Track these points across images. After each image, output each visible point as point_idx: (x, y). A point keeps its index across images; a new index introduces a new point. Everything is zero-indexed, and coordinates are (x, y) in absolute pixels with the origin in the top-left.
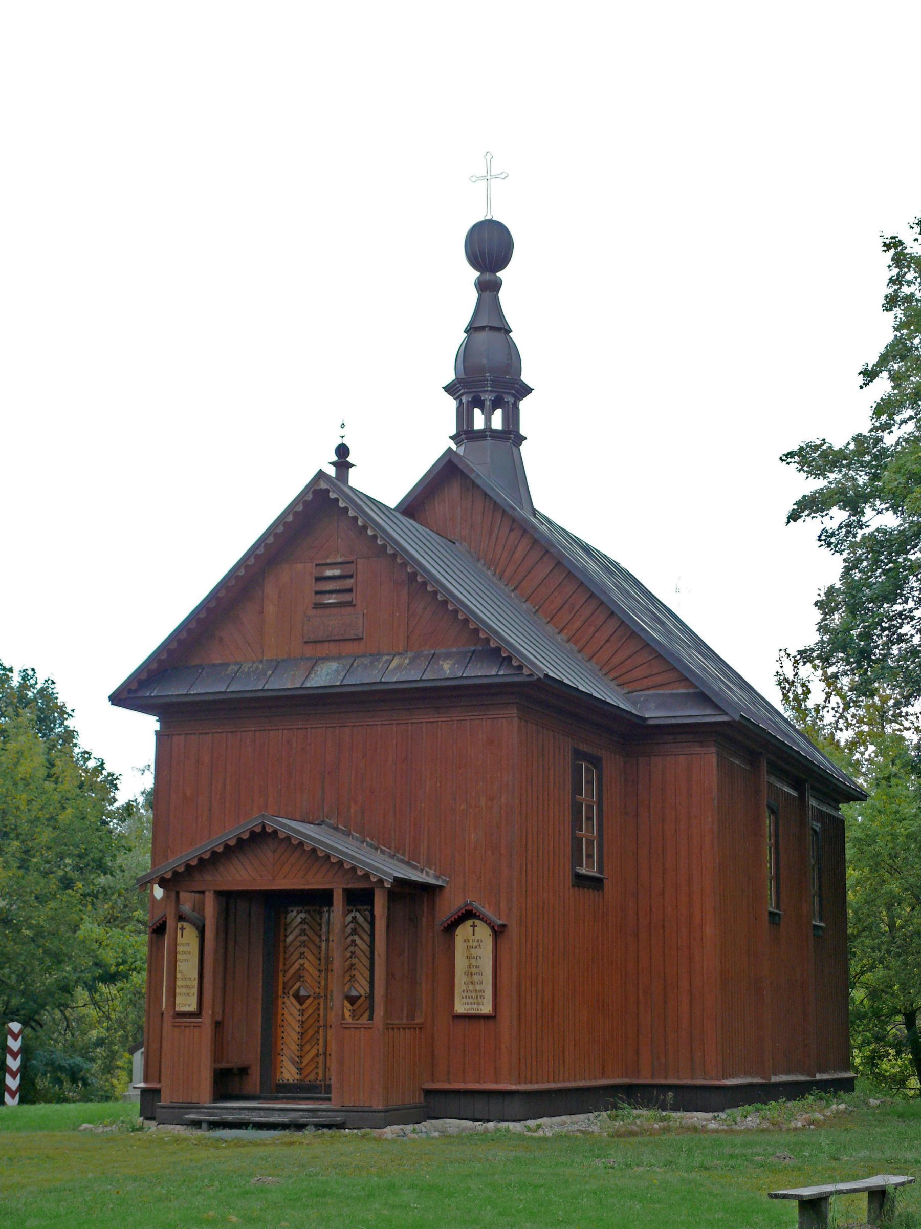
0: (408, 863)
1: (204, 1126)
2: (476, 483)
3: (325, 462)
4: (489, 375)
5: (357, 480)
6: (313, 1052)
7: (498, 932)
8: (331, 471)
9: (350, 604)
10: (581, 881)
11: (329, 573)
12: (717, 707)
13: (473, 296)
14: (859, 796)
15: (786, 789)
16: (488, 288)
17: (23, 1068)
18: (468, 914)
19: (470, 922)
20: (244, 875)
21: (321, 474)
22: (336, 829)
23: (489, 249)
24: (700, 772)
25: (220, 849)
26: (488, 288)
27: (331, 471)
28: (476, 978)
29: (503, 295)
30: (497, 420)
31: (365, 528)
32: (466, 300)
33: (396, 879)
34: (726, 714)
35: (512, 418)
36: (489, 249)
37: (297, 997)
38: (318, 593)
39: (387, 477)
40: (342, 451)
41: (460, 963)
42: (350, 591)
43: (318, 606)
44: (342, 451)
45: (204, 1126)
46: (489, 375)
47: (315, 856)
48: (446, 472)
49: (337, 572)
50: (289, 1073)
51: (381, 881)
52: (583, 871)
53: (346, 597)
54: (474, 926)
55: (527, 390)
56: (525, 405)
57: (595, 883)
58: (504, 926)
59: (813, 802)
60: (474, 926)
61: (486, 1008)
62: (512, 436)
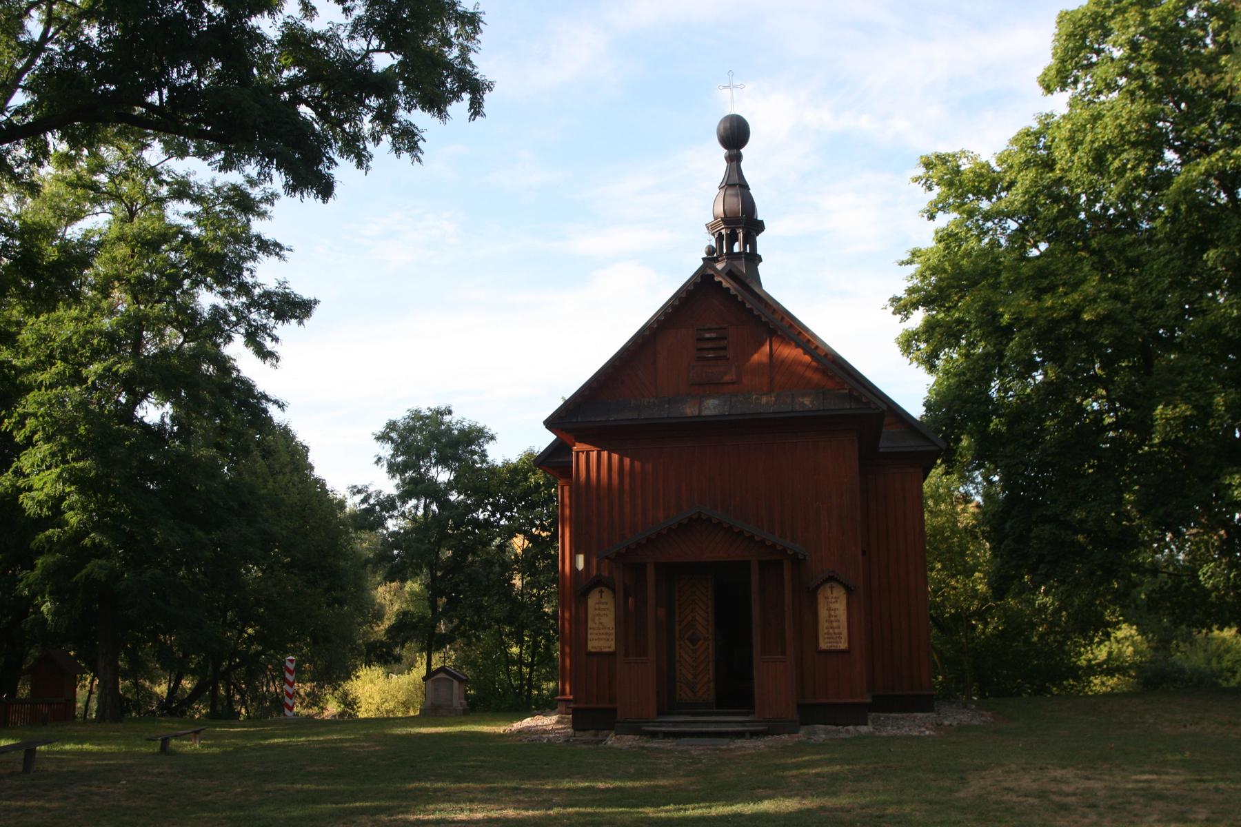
1: (748, 735)
7: (849, 591)
11: (707, 336)
13: (724, 165)
16: (734, 159)
19: (828, 585)
23: (735, 135)
26: (734, 159)
28: (835, 624)
36: (735, 135)
38: (699, 350)
41: (823, 614)
42: (725, 348)
43: (700, 359)
45: (748, 735)
46: (740, 223)
49: (714, 335)
53: (722, 353)
54: (601, 592)
60: (601, 592)
61: (843, 645)
62: (753, 259)
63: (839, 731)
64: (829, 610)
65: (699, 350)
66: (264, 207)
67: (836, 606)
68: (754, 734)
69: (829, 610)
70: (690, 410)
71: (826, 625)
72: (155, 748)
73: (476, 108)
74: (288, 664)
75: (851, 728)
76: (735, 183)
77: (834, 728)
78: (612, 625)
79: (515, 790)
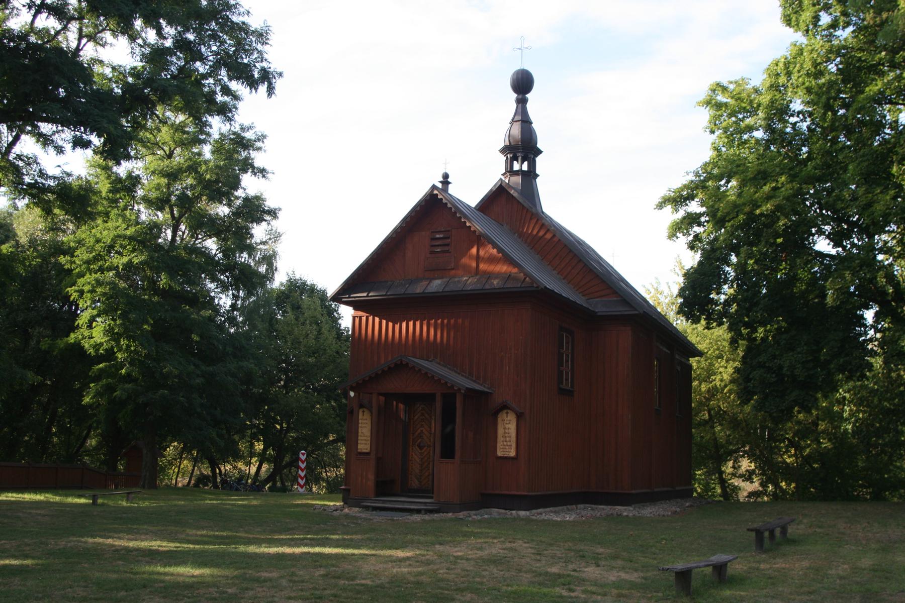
0: (475, 381)
2: (514, 203)
3: (437, 181)
4: (523, 147)
5: (452, 190)
6: (427, 474)
7: (519, 417)
8: (440, 186)
9: (448, 252)
10: (562, 392)
11: (438, 236)
12: (631, 306)
13: (514, 106)
14: (700, 354)
15: (665, 349)
16: (522, 102)
17: (307, 468)
18: (504, 407)
20: (395, 385)
21: (434, 187)
22: (439, 364)
23: (523, 84)
24: (623, 339)
25: (380, 372)
26: (522, 102)
27: (440, 186)
29: (528, 106)
30: (525, 167)
31: (455, 213)
32: (510, 106)
33: (467, 388)
34: (636, 310)
35: (532, 165)
36: (523, 84)
37: (419, 446)
39: (470, 192)
40: (446, 176)
41: (500, 431)
42: (448, 245)
43: (432, 253)
44: (446, 176)
46: (523, 147)
47: (427, 376)
48: (499, 194)
49: (441, 236)
50: (415, 483)
51: (459, 389)
52: (563, 386)
53: (446, 248)
55: (539, 152)
56: (539, 159)
57: (569, 393)
58: (522, 413)
59: (677, 357)
61: (513, 453)
63: (506, 514)
64: (505, 428)
65: (432, 246)
66: (258, 144)
67: (509, 426)
68: (431, 511)
69: (505, 428)
70: (419, 289)
71: (502, 439)
72: (100, 501)
73: (271, 91)
74: (301, 456)
75: (514, 512)
76: (523, 119)
77: (503, 511)
78: (369, 434)
79: (303, 539)
